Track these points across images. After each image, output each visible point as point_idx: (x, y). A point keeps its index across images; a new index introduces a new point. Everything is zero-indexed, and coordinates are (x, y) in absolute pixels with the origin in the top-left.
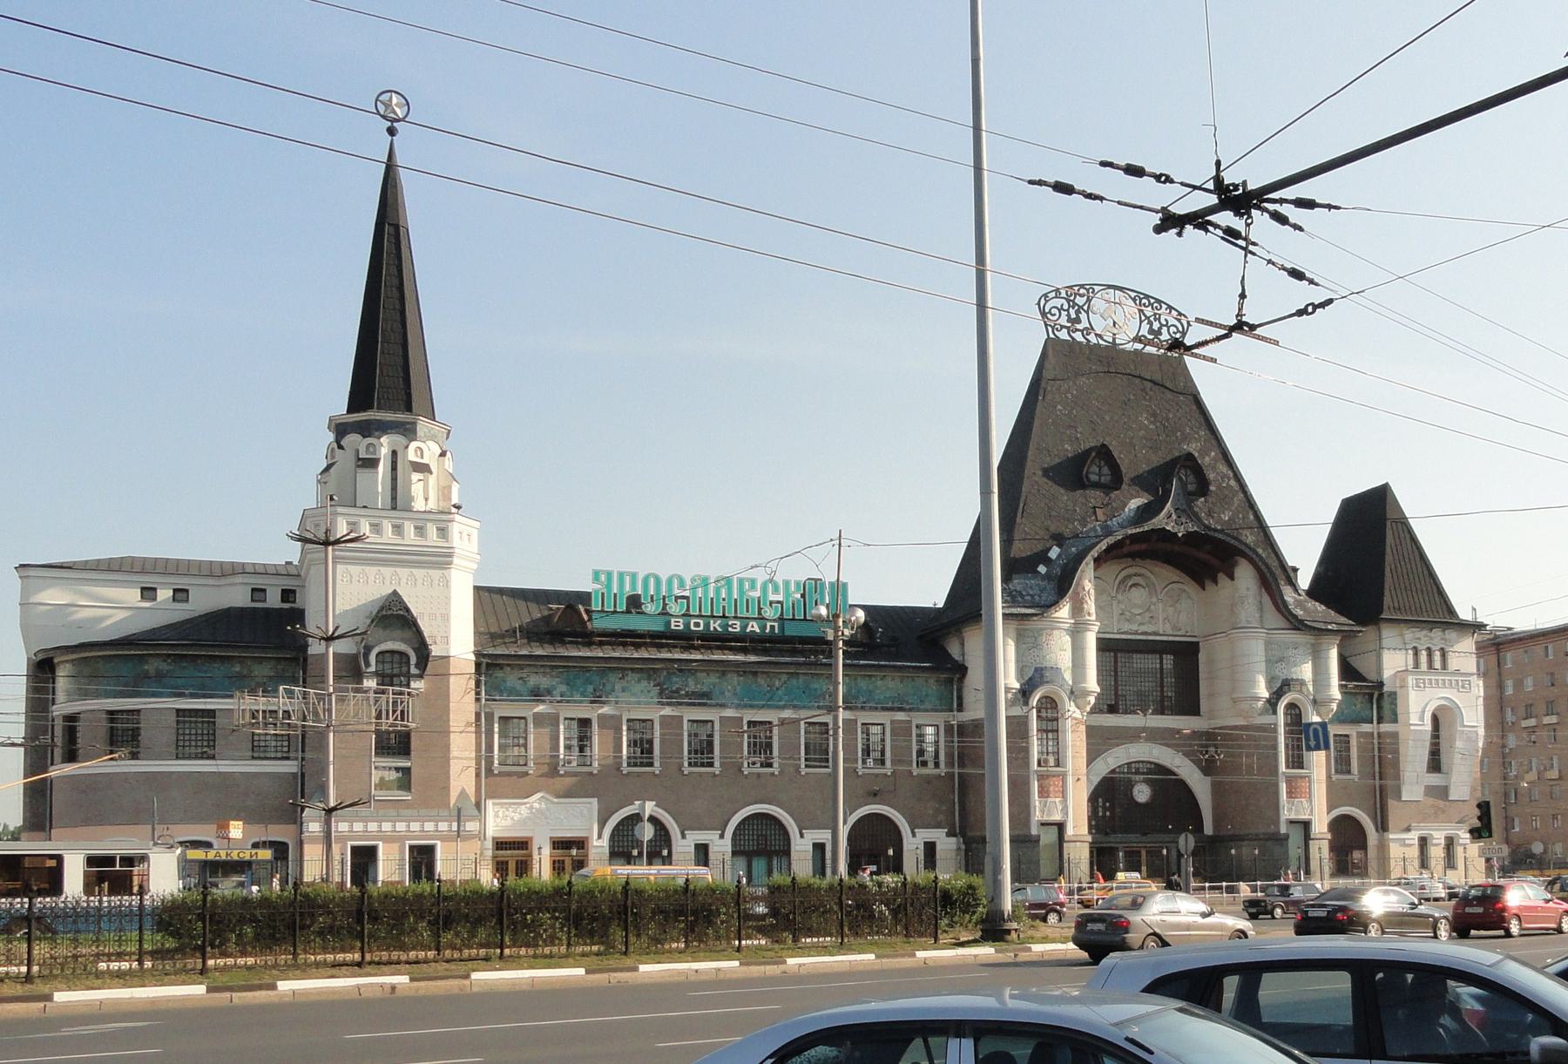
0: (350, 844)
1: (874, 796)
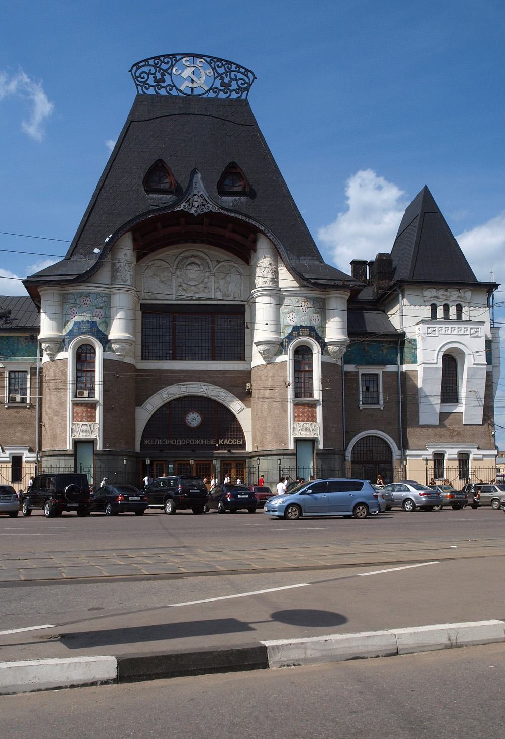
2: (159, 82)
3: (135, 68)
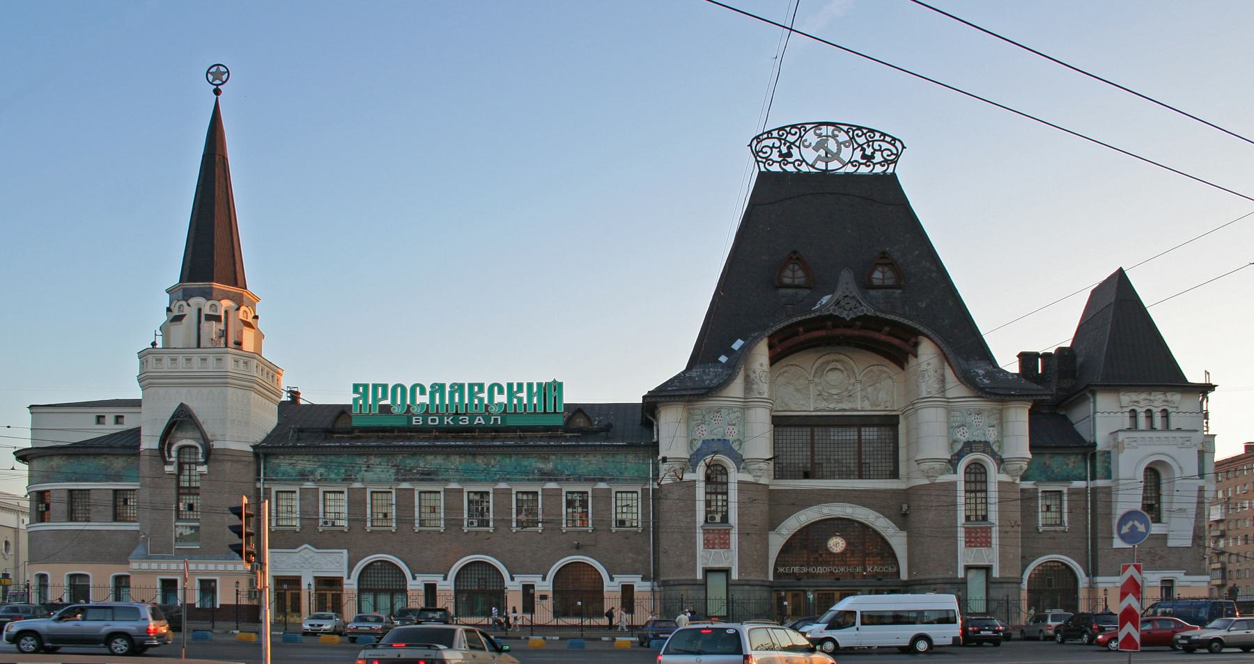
0: (159, 577)
1: (578, 548)
2: (785, 156)
3: (755, 142)
